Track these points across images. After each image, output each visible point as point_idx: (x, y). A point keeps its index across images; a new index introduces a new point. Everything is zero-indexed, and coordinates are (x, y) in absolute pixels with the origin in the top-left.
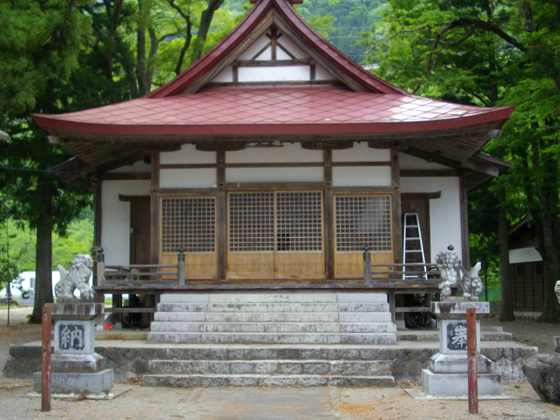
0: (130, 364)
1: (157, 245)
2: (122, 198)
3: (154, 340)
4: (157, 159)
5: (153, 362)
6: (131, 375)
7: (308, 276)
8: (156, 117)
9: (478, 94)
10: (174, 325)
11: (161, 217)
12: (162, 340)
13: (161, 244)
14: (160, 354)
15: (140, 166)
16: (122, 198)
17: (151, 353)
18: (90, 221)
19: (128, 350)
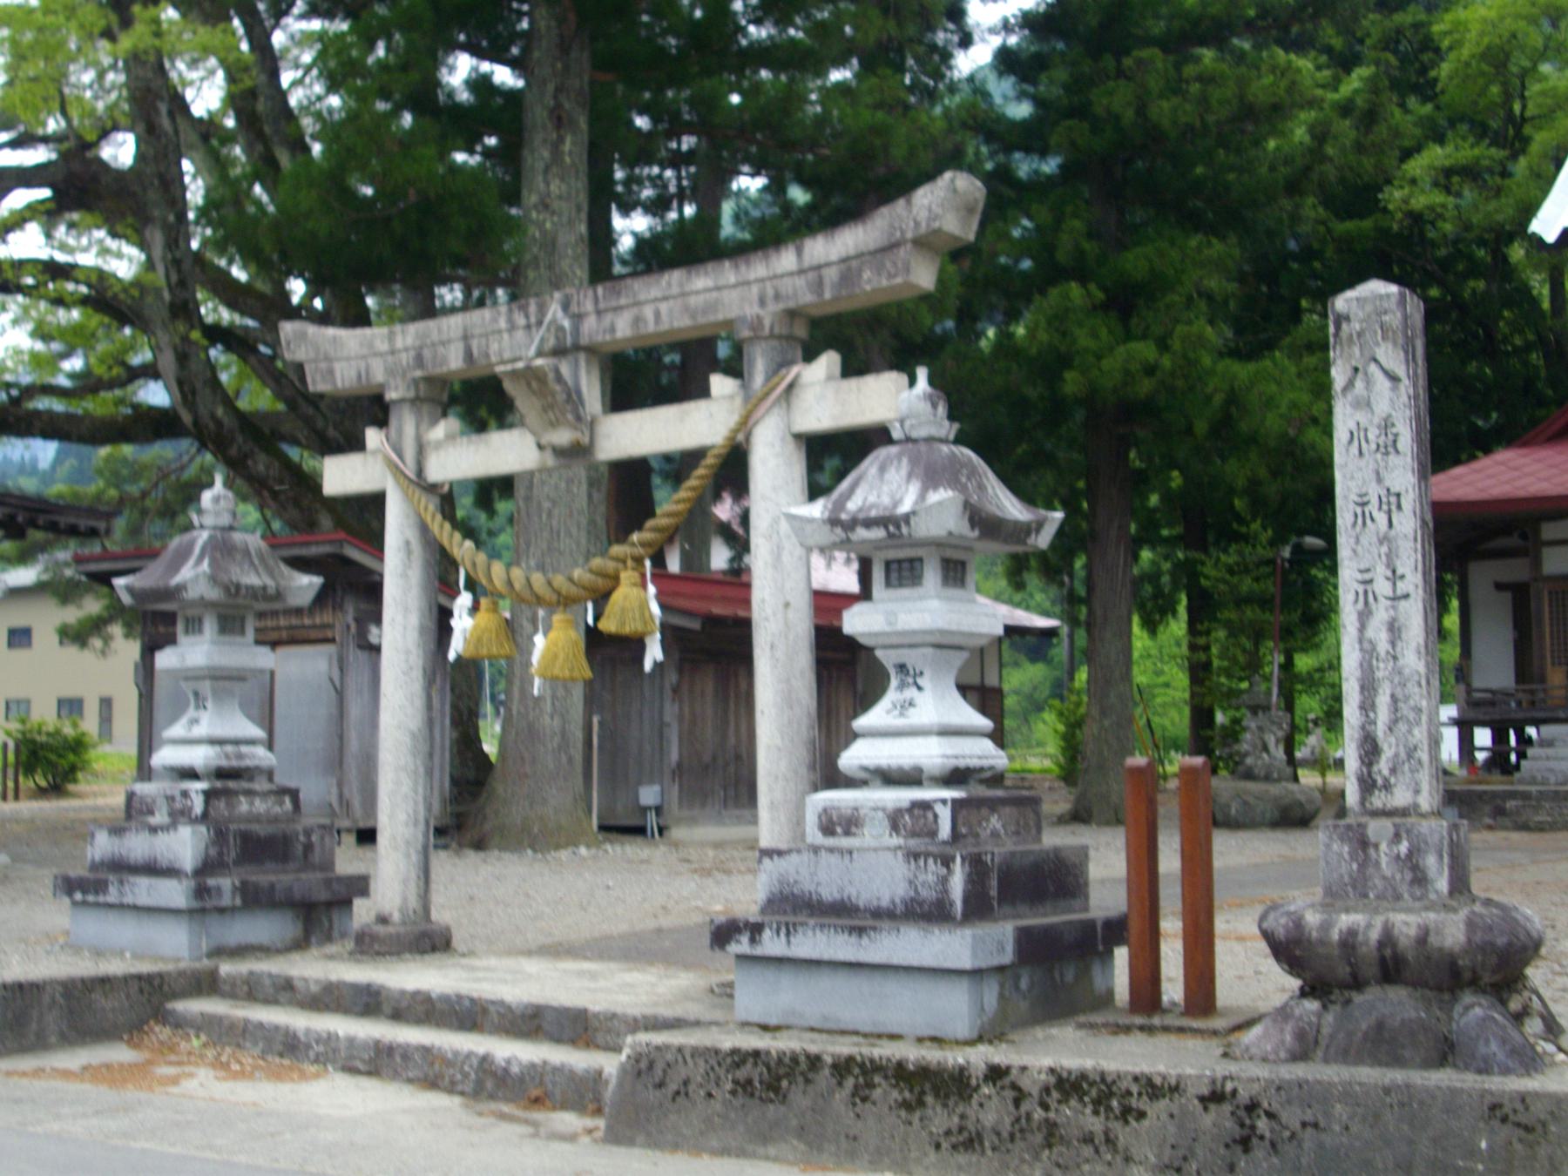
0: (1487, 809)
1: (1543, 657)
2: (1499, 586)
3: (1521, 782)
4: (1537, 532)
5: (1511, 804)
6: (1488, 821)
7: (288, 344)
8: (1518, 484)
9: (101, 899)
10: (1552, 764)
11: (1547, 615)
12: (1533, 781)
13: (1548, 655)
14: (1526, 796)
15: (1513, 541)
16: (1499, 586)
17: (1513, 795)
18: (848, 561)
19: (1485, 792)
